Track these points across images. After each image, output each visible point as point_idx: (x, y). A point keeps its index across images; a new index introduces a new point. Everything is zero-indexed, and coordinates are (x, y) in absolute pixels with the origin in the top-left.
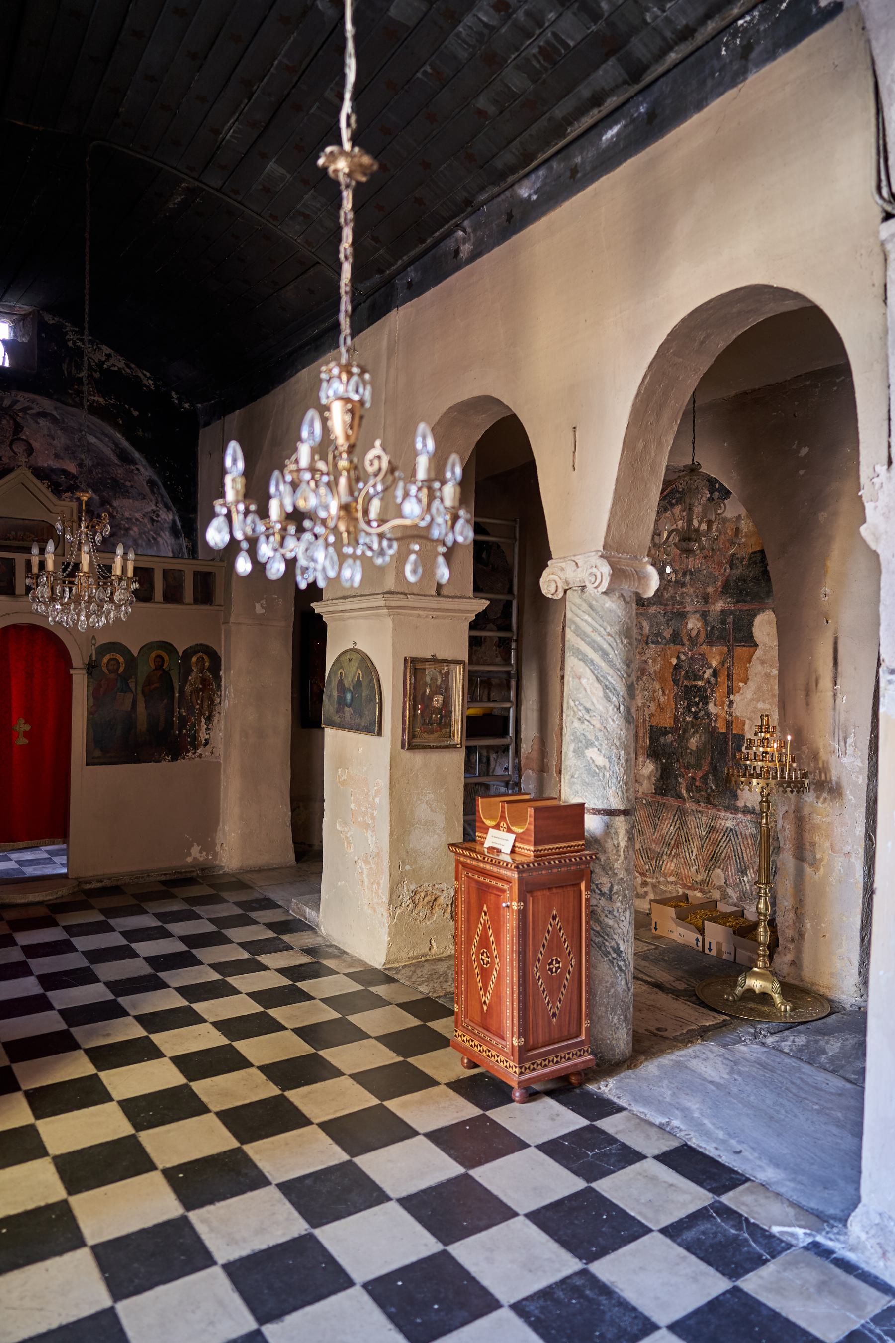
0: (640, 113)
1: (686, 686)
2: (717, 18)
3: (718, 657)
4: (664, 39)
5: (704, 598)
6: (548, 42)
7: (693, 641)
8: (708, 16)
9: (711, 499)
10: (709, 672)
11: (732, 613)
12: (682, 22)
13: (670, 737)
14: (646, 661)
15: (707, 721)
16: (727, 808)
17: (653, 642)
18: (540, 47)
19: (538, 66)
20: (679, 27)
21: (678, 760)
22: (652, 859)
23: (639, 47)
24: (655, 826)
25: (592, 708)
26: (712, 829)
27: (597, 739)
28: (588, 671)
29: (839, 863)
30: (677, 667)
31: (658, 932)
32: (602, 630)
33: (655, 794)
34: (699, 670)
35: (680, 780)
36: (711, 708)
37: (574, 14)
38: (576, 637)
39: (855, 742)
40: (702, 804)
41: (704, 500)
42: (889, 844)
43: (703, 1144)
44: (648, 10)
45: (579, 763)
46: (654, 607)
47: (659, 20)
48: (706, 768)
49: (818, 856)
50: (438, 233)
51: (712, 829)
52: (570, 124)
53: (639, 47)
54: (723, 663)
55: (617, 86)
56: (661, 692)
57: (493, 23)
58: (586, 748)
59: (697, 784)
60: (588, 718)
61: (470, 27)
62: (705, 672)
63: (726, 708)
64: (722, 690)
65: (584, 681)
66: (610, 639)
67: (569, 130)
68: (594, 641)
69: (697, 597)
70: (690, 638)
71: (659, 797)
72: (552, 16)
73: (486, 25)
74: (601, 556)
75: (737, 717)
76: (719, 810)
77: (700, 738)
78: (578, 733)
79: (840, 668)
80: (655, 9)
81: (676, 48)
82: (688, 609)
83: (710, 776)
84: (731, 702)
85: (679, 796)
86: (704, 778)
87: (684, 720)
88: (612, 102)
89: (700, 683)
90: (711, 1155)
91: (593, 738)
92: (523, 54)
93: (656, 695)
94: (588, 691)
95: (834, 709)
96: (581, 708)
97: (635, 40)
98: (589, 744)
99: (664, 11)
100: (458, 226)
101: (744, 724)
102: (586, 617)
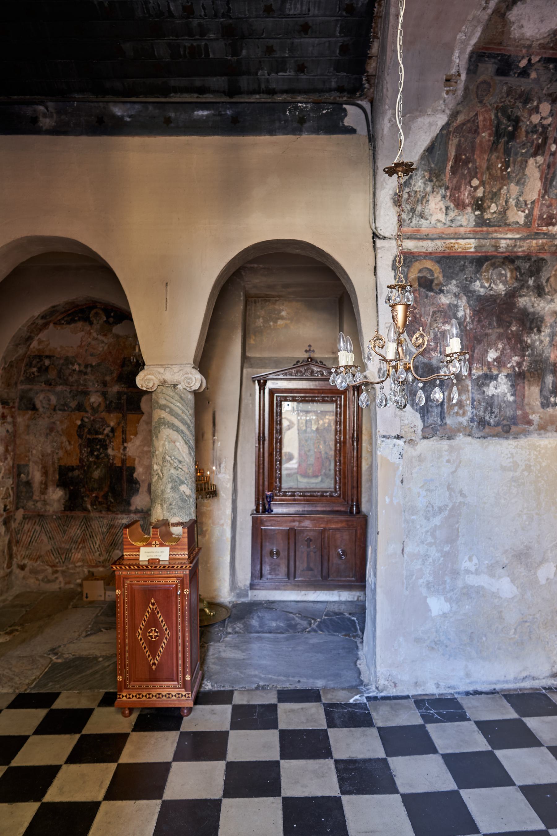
0: (226, 114)
1: (89, 439)
2: (290, 95)
3: (115, 420)
4: (259, 86)
5: (103, 383)
6: (199, 46)
7: (95, 410)
8: (286, 92)
9: (107, 322)
10: (107, 430)
11: (125, 393)
12: (273, 85)
13: (76, 472)
14: (54, 423)
15: (107, 460)
16: (123, 512)
17: (60, 410)
18: (192, 45)
19: (182, 53)
20: (270, 87)
21: (84, 486)
22: (62, 554)
23: (244, 82)
24: (65, 532)
25: (183, 460)
26: (111, 526)
27: (186, 479)
28: (180, 438)
29: (217, 531)
30: (81, 427)
31: (88, 599)
32: (187, 412)
33: (65, 510)
34: (99, 428)
35: (86, 499)
36: (110, 451)
37: (225, 44)
38: (170, 417)
39: (226, 466)
40: (104, 512)
41: (101, 321)
42: (384, 511)
43: (284, 686)
44: (262, 69)
45: (176, 495)
46: (61, 387)
47: (263, 77)
48: (106, 489)
49: (204, 529)
50: (16, 97)
51: (111, 526)
52: (176, 92)
53: (244, 82)
54: (119, 424)
55: (218, 92)
56: (67, 443)
57: (176, 14)
58: (180, 485)
59: (100, 500)
60: (181, 467)
61: (159, 5)
62: (104, 429)
63: (121, 451)
64: (119, 440)
65: (178, 444)
66: (190, 417)
67: (172, 95)
68: (183, 419)
69: (97, 382)
70: (93, 408)
71: (68, 513)
72: (212, 36)
73: (169, 11)
74: (193, 368)
75: (130, 457)
76: (117, 514)
77: (101, 471)
78: (174, 477)
79: (217, 428)
80: (266, 72)
81: (262, 95)
82: (90, 389)
83: (110, 494)
84: (125, 448)
85: (85, 510)
86: (105, 496)
87: (88, 460)
88: (209, 98)
89: (100, 437)
90: (292, 689)
91: (184, 479)
92: (178, 41)
93: (63, 445)
94: (181, 450)
95: (213, 449)
96: (175, 461)
97: (245, 78)
98: (182, 483)
99: (269, 75)
100: (42, 103)
101: (134, 460)
102: (178, 404)
